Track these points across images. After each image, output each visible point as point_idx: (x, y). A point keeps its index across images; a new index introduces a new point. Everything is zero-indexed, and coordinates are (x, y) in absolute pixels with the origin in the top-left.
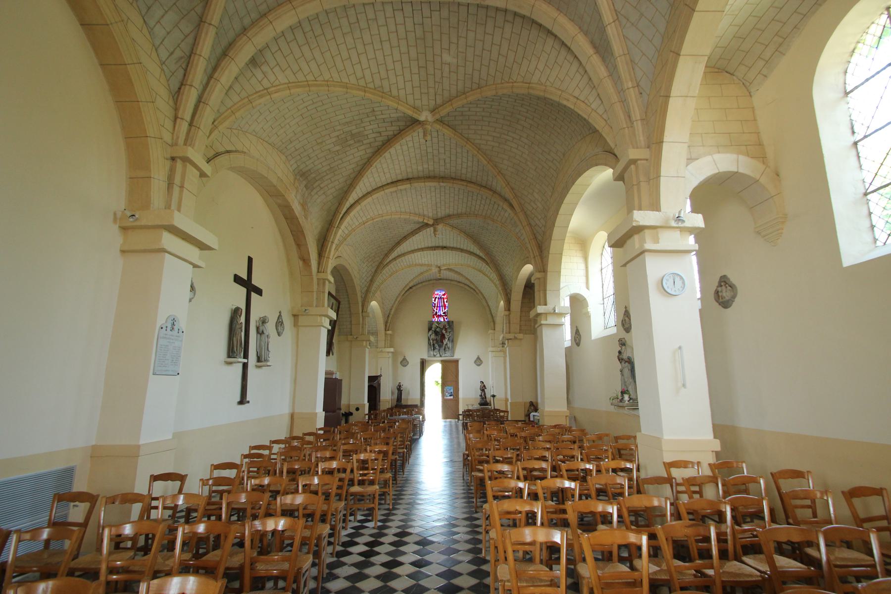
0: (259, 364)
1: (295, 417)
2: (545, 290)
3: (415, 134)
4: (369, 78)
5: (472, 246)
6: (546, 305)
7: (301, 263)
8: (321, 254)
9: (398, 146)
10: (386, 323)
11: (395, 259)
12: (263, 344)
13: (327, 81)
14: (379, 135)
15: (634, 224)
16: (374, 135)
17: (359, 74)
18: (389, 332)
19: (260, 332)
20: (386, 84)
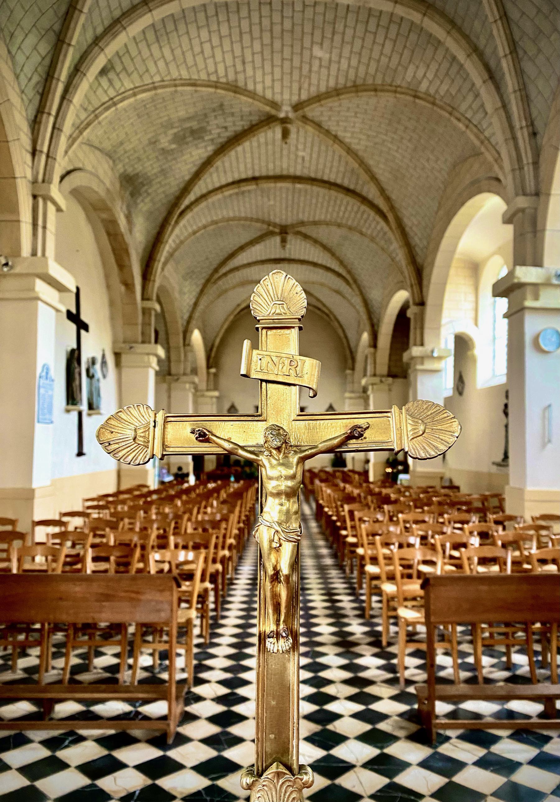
0: (91, 412)
1: (122, 473)
2: (422, 328)
3: (270, 134)
4: (221, 72)
5: (330, 261)
6: (422, 344)
7: (123, 288)
8: (146, 275)
9: (247, 144)
10: (208, 358)
11: (225, 274)
12: (94, 389)
13: (175, 80)
14: (224, 130)
15: (516, 281)
16: (218, 131)
17: (211, 69)
18: (213, 370)
19: (90, 376)
20: (241, 77)
